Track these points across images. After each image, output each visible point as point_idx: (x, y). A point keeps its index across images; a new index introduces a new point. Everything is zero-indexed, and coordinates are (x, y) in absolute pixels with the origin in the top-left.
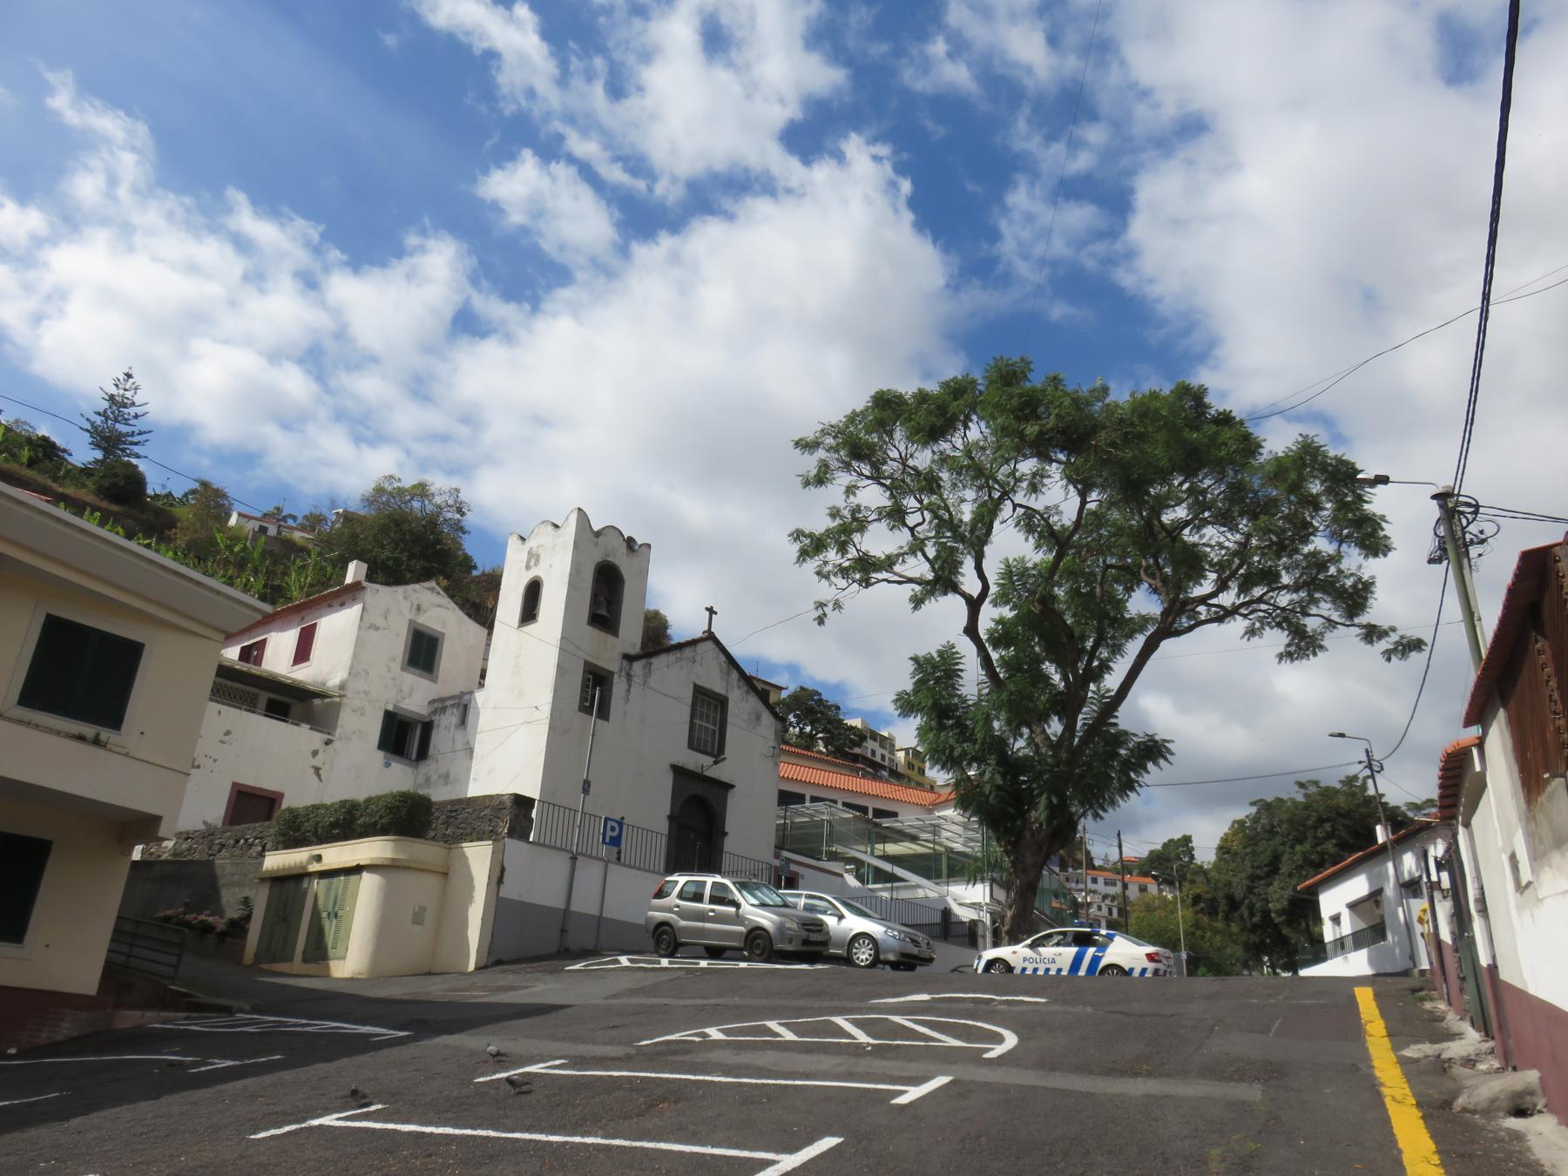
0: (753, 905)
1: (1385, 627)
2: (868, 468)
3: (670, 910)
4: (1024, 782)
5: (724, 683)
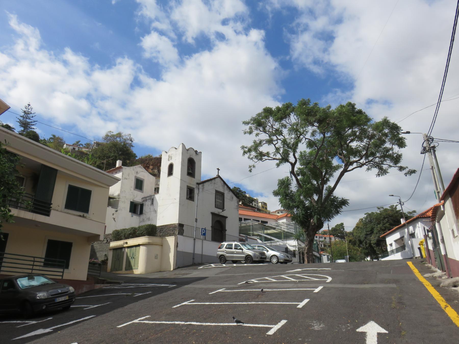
0: (246, 249)
1: (405, 167)
2: (262, 128)
3: (223, 252)
4: (309, 212)
5: (223, 189)
